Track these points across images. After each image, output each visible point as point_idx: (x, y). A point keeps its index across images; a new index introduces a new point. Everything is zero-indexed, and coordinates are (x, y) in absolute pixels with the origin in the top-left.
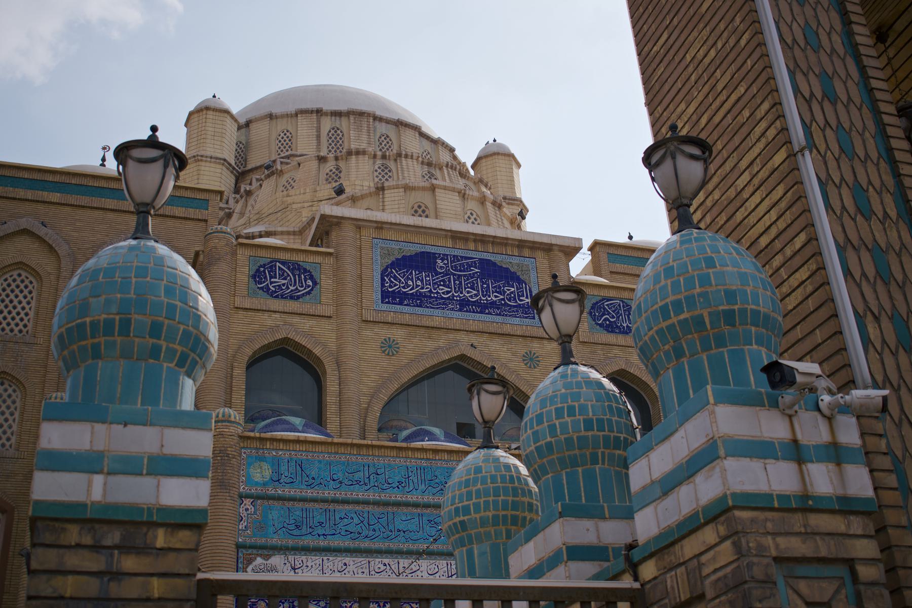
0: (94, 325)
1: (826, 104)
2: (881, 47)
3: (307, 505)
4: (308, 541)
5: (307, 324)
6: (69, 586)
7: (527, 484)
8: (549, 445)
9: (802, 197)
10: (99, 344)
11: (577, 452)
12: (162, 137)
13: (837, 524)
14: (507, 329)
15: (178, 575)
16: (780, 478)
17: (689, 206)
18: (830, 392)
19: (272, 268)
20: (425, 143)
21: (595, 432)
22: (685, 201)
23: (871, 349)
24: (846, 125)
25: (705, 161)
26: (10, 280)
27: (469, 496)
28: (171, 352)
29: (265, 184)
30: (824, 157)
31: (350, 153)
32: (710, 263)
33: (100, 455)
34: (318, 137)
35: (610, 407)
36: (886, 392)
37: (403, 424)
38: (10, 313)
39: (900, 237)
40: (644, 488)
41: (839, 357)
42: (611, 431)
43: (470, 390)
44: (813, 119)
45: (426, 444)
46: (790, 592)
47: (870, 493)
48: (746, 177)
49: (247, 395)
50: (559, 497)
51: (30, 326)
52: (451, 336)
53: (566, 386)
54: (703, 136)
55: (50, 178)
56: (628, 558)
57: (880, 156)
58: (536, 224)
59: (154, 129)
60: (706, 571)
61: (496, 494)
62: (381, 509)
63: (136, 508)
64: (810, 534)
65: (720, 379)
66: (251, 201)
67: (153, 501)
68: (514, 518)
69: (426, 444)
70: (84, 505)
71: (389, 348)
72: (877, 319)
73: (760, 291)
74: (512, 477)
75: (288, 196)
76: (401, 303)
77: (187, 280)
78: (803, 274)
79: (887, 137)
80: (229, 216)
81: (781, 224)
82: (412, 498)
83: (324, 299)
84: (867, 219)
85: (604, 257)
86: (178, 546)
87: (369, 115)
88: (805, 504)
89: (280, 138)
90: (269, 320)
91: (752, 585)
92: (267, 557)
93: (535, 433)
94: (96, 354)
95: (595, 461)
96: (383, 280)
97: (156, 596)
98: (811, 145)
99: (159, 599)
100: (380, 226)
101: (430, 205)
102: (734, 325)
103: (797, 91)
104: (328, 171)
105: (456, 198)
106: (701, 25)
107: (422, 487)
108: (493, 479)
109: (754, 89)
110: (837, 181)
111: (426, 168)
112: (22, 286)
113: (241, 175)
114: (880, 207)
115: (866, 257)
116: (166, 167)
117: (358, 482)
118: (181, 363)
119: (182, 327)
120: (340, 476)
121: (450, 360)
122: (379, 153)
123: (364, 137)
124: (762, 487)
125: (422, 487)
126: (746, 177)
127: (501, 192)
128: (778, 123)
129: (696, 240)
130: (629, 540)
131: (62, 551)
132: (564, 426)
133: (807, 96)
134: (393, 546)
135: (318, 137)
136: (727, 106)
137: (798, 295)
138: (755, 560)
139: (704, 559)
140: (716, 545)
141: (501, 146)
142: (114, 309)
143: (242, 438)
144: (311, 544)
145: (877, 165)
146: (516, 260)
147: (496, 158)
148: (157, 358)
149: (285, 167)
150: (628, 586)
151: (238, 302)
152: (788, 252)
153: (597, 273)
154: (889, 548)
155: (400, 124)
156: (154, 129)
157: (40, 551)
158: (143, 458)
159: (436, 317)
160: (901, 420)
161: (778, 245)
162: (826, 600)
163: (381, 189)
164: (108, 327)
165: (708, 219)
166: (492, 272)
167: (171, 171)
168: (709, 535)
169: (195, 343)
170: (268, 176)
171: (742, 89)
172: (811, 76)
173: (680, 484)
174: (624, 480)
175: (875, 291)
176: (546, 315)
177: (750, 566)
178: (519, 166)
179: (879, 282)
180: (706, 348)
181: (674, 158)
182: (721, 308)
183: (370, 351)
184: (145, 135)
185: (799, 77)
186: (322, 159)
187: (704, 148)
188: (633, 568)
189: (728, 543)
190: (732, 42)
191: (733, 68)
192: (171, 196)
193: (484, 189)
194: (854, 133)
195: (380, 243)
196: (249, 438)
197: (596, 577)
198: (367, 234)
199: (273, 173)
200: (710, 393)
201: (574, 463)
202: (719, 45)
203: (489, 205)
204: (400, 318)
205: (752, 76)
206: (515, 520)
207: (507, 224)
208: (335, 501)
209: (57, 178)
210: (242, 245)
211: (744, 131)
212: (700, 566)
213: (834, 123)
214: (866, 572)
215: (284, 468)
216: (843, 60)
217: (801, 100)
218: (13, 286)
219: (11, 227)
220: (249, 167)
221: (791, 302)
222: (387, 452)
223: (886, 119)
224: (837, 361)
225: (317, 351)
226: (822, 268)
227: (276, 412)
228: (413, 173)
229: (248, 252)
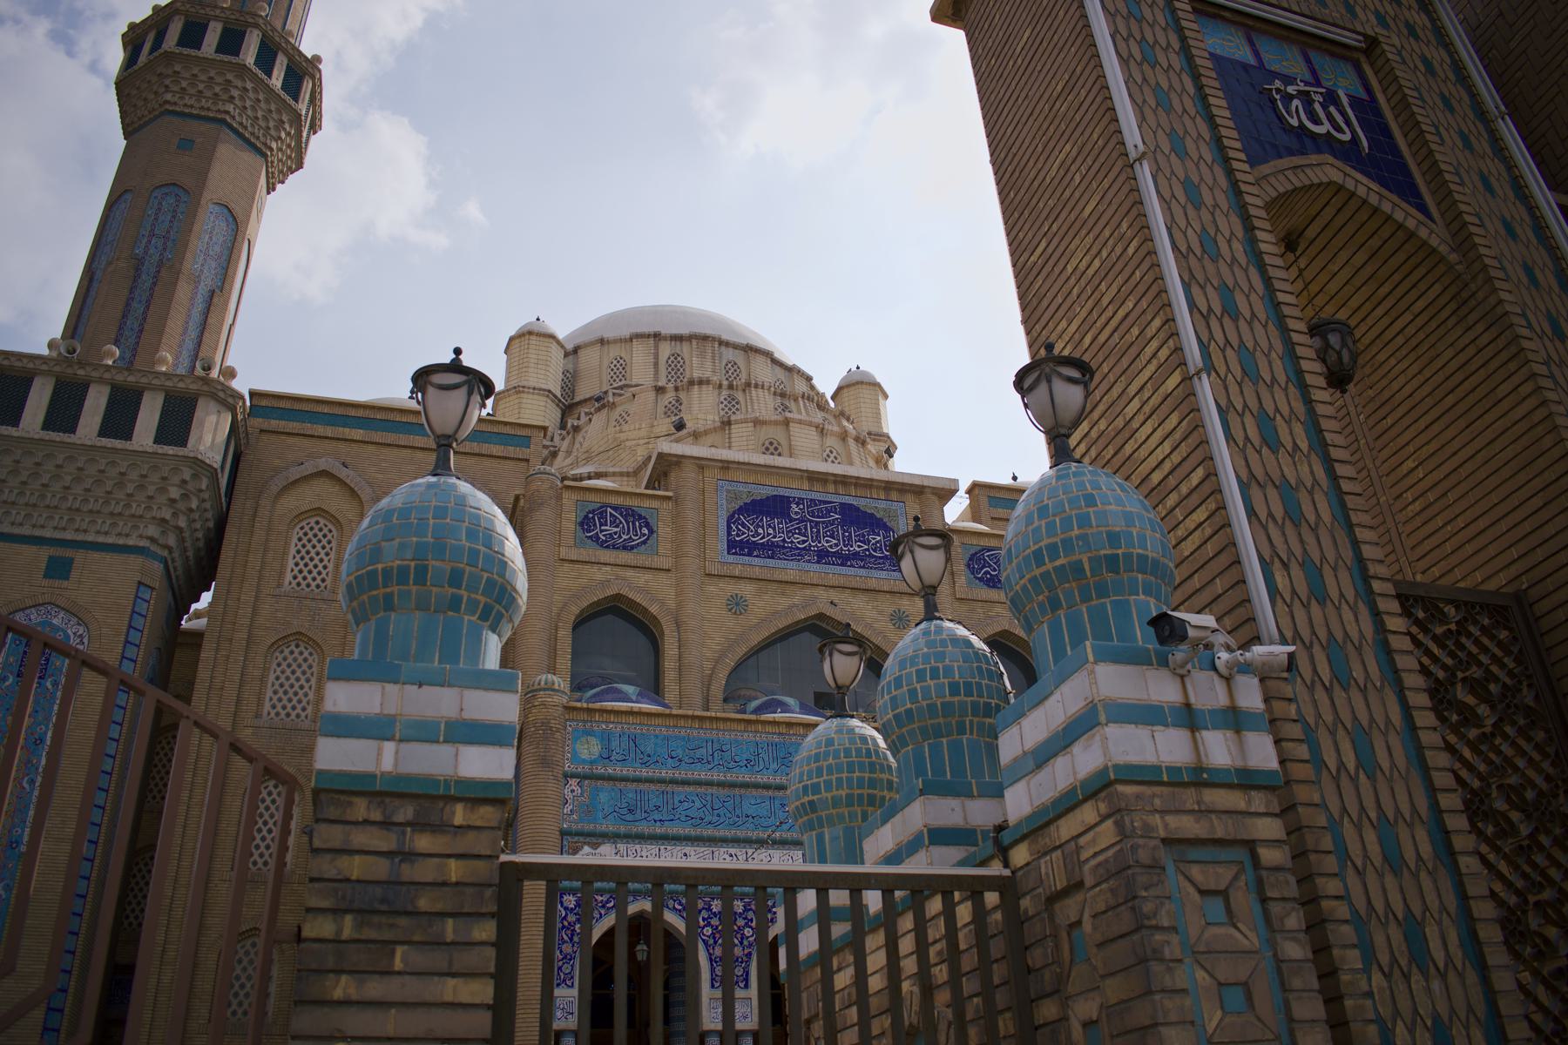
0: (387, 572)
1: (1226, 320)
2: (1291, 257)
3: (642, 786)
4: (643, 828)
5: (642, 578)
6: (356, 867)
7: (886, 759)
8: (909, 712)
9: (1198, 426)
10: (392, 594)
11: (941, 720)
12: (466, 361)
13: (1235, 800)
14: (873, 584)
15: (478, 857)
16: (1168, 748)
17: (1068, 436)
18: (1229, 649)
19: (602, 515)
20: (778, 369)
21: (962, 698)
22: (1063, 431)
23: (1279, 601)
24: (1250, 345)
25: (1086, 386)
26: (307, 529)
27: (819, 771)
28: (473, 604)
29: (595, 418)
30: (1224, 381)
31: (691, 383)
32: (1090, 500)
33: (390, 720)
34: (656, 364)
35: (979, 669)
36: (1291, 648)
37: (753, 694)
38: (306, 565)
39: (1312, 472)
40: (1015, 760)
41: (1242, 609)
42: (980, 695)
43: (821, 651)
44: (1212, 337)
45: (779, 716)
46: (1181, 878)
47: (1274, 764)
48: (1136, 404)
49: (573, 659)
50: (920, 772)
51: (329, 581)
52: (808, 592)
53: (930, 644)
54: (1086, 358)
55: (353, 413)
56: (997, 841)
57: (1288, 380)
58: (904, 464)
59: (458, 351)
60: (1085, 855)
61: (851, 769)
62: (726, 791)
63: (430, 780)
64: (1204, 812)
65: (1102, 633)
66: (579, 438)
67: (450, 772)
68: (871, 798)
69: (779, 716)
70: (372, 776)
71: (737, 605)
72: (1285, 566)
73: (1148, 533)
74: (868, 750)
76: (749, 555)
77: (492, 522)
78: (1200, 515)
79: (1295, 358)
80: (554, 455)
81: (1176, 458)
82: (760, 779)
83: (661, 550)
84: (1275, 452)
85: (984, 501)
86: (478, 823)
87: (714, 339)
88: (1199, 777)
90: (599, 574)
91: (1138, 870)
92: (595, 846)
93: (893, 699)
94: (389, 606)
95: (961, 731)
96: (729, 528)
97: (454, 880)
98: (1209, 367)
99: (457, 884)
100: (726, 465)
101: (784, 442)
102: (1118, 573)
103: (1192, 305)
105: (813, 432)
106: (1084, 232)
107: (774, 766)
108: (847, 752)
109: (1144, 304)
110: (1239, 408)
111: (779, 400)
112: (320, 535)
113: (568, 408)
114: (1289, 438)
115: (1272, 494)
116: (470, 394)
117: (700, 760)
118: (484, 617)
119: (486, 575)
120: (680, 752)
121: (806, 620)
122: (725, 383)
123: (709, 364)
124: (1149, 758)
125: (774, 766)
126: (1136, 404)
127: (866, 426)
128: (1171, 342)
129: (1075, 474)
130: (998, 821)
131: (348, 828)
132: (926, 691)
133: (1205, 311)
134: (740, 834)
135: (656, 364)
136: (1114, 323)
137: (1196, 539)
138: (1141, 841)
139: (1082, 841)
140: (1096, 825)
141: (865, 373)
142: (409, 555)
143: (567, 708)
144: (646, 831)
145: (1286, 390)
146: (882, 505)
147: (860, 387)
148: (457, 610)
149: (617, 399)
150: (997, 873)
151: (564, 553)
152: (1184, 489)
153: (976, 519)
154: (1299, 829)
155: (750, 350)
156: (458, 351)
157: (323, 827)
158: (439, 723)
159: (791, 570)
160: (1313, 682)
161: (1172, 481)
162: (1222, 887)
163: (727, 424)
164: (403, 573)
165: (1093, 453)
166: (854, 517)
167: (477, 398)
168: (1088, 814)
169: (502, 593)
170: (599, 410)
171: (1130, 304)
172: (1209, 289)
173: (1055, 755)
174: (993, 751)
175: (1284, 534)
176: (906, 564)
177: (1134, 848)
178: (886, 397)
179: (1288, 522)
180: (1086, 599)
181: (1049, 381)
182: (1102, 552)
183: (713, 610)
184: (447, 358)
185: (1195, 290)
186: (660, 390)
187: (1084, 370)
188: (1003, 852)
189: (1109, 823)
190: (1118, 250)
191: (1120, 280)
192: (474, 431)
193: (845, 423)
194: (1258, 354)
195: (727, 486)
196: (575, 709)
197: (962, 863)
198: (711, 476)
199: (604, 406)
200: (1089, 650)
201: (938, 733)
202: (1104, 254)
203: (851, 442)
204: (749, 572)
205: (1141, 288)
206: (872, 801)
207: (872, 463)
208: (673, 782)
209: (360, 413)
210: (568, 487)
211: (1133, 351)
212: (1078, 849)
213: (1235, 344)
214: (1268, 856)
215: (614, 744)
216: (1246, 271)
217: (1197, 316)
218: (310, 535)
219: (308, 468)
220: (577, 399)
221: (1188, 547)
222: (735, 726)
223: (1295, 337)
224: (1241, 613)
225: (654, 609)
226: (1222, 507)
227: (606, 679)
228: (764, 405)
229: (575, 496)
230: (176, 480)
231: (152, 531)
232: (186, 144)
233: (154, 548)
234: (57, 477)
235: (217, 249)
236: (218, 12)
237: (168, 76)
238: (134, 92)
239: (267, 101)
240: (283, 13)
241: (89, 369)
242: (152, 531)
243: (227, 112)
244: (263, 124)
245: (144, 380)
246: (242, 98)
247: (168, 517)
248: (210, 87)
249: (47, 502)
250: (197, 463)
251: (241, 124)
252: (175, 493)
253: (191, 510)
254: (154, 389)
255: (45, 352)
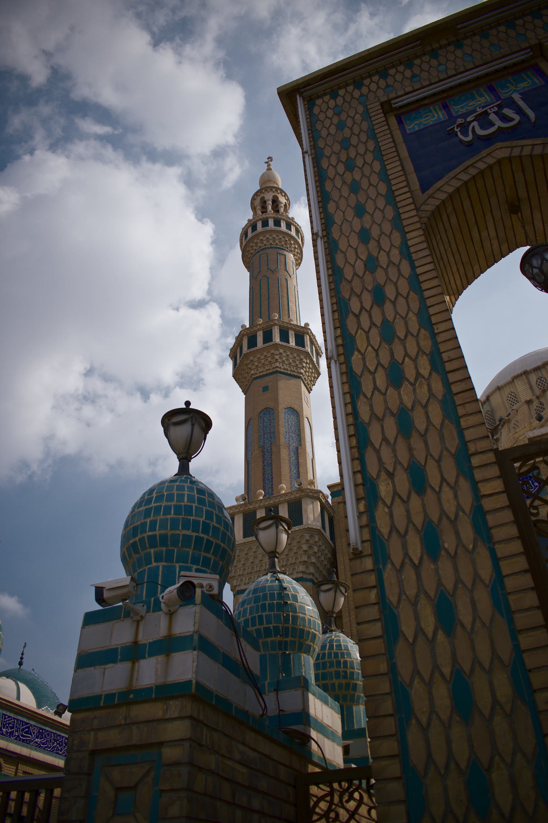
75: (516, 433)
89: (509, 399)
104: (535, 407)
199: (504, 423)
230: (304, 541)
231: (302, 568)
232: (265, 389)
233: (305, 576)
234: (255, 557)
235: (293, 428)
236: (258, 327)
237: (249, 363)
238: (240, 376)
239: (292, 354)
240: (287, 312)
241: (253, 504)
242: (302, 568)
243: (277, 367)
244: (293, 364)
245: (277, 500)
246: (281, 358)
247: (306, 560)
248: (266, 360)
249: (238, 573)
250: (311, 530)
251: (285, 369)
252: (305, 547)
253: (315, 553)
254: (281, 503)
255: (235, 503)
